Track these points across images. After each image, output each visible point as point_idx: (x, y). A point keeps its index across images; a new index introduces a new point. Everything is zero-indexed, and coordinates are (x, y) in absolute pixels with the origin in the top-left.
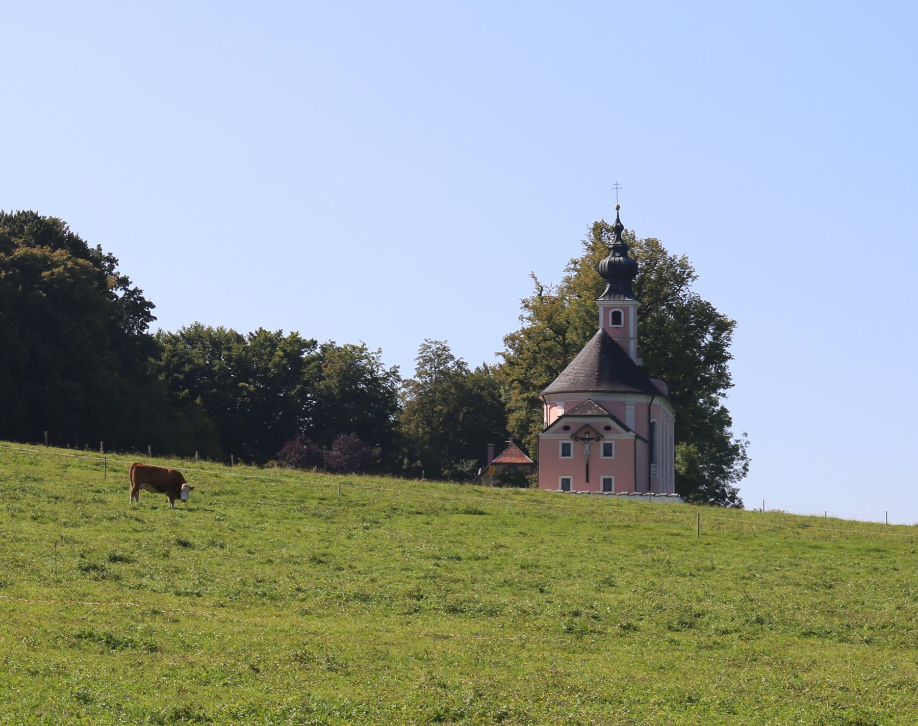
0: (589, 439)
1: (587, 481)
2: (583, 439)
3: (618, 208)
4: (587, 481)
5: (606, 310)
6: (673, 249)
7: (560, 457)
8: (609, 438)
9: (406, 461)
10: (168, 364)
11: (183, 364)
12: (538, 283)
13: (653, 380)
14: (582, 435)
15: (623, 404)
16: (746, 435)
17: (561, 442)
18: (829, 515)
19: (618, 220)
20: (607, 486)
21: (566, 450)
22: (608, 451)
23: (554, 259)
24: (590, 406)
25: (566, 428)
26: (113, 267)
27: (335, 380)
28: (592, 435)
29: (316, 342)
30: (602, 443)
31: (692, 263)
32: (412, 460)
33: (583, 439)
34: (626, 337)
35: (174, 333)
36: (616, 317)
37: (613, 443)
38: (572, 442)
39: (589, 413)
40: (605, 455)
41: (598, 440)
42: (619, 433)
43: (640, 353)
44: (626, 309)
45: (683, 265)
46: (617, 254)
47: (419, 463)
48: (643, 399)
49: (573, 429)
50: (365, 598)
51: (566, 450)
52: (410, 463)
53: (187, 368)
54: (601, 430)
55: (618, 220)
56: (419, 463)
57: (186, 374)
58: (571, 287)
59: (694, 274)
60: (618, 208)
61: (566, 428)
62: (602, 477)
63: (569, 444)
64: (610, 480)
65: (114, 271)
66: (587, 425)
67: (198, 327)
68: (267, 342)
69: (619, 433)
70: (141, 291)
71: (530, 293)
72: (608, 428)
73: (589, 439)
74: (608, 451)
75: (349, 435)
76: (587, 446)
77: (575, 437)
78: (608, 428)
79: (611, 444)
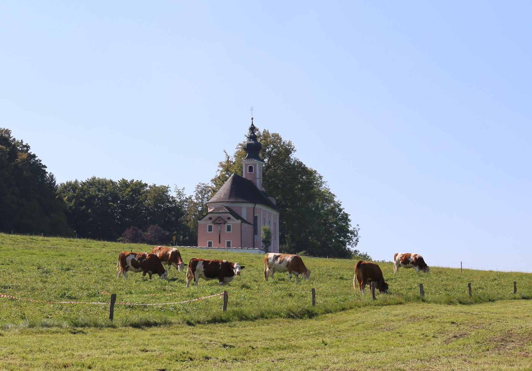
0: (220, 224)
3: (252, 119)
5: (246, 165)
6: (285, 139)
8: (230, 223)
9: (181, 237)
10: (78, 195)
11: (84, 195)
12: (227, 155)
13: (269, 198)
14: (217, 222)
15: (241, 208)
16: (358, 225)
18: (464, 267)
19: (252, 125)
20: (229, 244)
21: (210, 229)
22: (229, 229)
23: (231, 143)
24: (221, 208)
25: (210, 219)
26: (28, 150)
27: (152, 201)
28: (222, 221)
29: (147, 184)
30: (226, 225)
31: (294, 144)
32: (184, 236)
34: (255, 178)
35: (84, 181)
36: (251, 169)
38: (213, 225)
39: (221, 211)
40: (209, 231)
41: (224, 224)
42: (234, 220)
43: (263, 185)
44: (255, 165)
45: (289, 145)
47: (187, 238)
48: (251, 205)
49: (213, 219)
50: (472, 314)
51: (210, 229)
52: (183, 238)
53: (86, 197)
54: (226, 219)
55: (252, 125)
56: (187, 238)
57: (86, 199)
58: (238, 155)
59: (294, 149)
60: (252, 119)
61: (210, 219)
62: (226, 241)
63: (211, 226)
64: (230, 242)
65: (29, 152)
66: (219, 217)
67: (94, 178)
68: (93, 183)
69: (234, 220)
70: (41, 161)
71: (224, 160)
72: (229, 218)
73: (220, 224)
74: (229, 229)
75: (155, 225)
77: (214, 222)
78: (229, 218)
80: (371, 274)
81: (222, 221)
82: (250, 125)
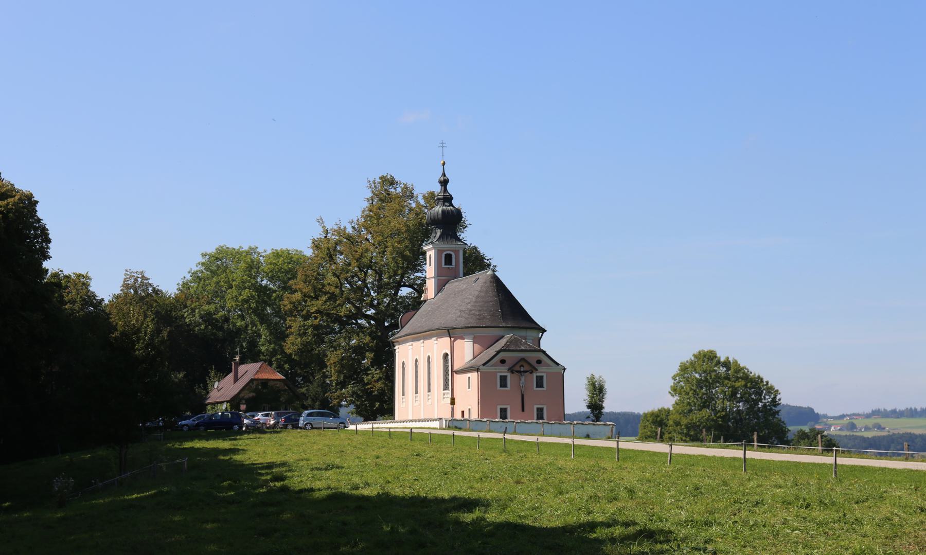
1: (523, 410)
2: (519, 372)
4: (523, 410)
7: (499, 388)
14: (517, 368)
17: (499, 375)
21: (503, 383)
22: (540, 383)
25: (503, 362)
28: (527, 368)
30: (535, 375)
33: (519, 372)
37: (544, 375)
38: (508, 375)
39: (523, 348)
46: (447, 204)
51: (503, 383)
54: (534, 363)
60: (444, 164)
61: (503, 362)
62: (536, 407)
66: (523, 359)
71: (318, 234)
74: (540, 383)
76: (523, 379)
77: (511, 370)
79: (542, 377)
80: (478, 370)
81: (527, 368)
82: (438, 176)
